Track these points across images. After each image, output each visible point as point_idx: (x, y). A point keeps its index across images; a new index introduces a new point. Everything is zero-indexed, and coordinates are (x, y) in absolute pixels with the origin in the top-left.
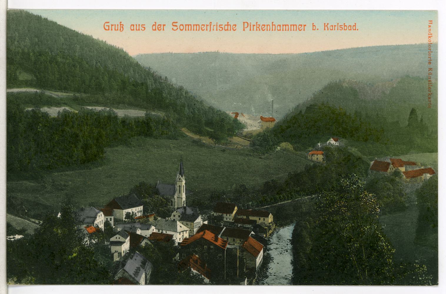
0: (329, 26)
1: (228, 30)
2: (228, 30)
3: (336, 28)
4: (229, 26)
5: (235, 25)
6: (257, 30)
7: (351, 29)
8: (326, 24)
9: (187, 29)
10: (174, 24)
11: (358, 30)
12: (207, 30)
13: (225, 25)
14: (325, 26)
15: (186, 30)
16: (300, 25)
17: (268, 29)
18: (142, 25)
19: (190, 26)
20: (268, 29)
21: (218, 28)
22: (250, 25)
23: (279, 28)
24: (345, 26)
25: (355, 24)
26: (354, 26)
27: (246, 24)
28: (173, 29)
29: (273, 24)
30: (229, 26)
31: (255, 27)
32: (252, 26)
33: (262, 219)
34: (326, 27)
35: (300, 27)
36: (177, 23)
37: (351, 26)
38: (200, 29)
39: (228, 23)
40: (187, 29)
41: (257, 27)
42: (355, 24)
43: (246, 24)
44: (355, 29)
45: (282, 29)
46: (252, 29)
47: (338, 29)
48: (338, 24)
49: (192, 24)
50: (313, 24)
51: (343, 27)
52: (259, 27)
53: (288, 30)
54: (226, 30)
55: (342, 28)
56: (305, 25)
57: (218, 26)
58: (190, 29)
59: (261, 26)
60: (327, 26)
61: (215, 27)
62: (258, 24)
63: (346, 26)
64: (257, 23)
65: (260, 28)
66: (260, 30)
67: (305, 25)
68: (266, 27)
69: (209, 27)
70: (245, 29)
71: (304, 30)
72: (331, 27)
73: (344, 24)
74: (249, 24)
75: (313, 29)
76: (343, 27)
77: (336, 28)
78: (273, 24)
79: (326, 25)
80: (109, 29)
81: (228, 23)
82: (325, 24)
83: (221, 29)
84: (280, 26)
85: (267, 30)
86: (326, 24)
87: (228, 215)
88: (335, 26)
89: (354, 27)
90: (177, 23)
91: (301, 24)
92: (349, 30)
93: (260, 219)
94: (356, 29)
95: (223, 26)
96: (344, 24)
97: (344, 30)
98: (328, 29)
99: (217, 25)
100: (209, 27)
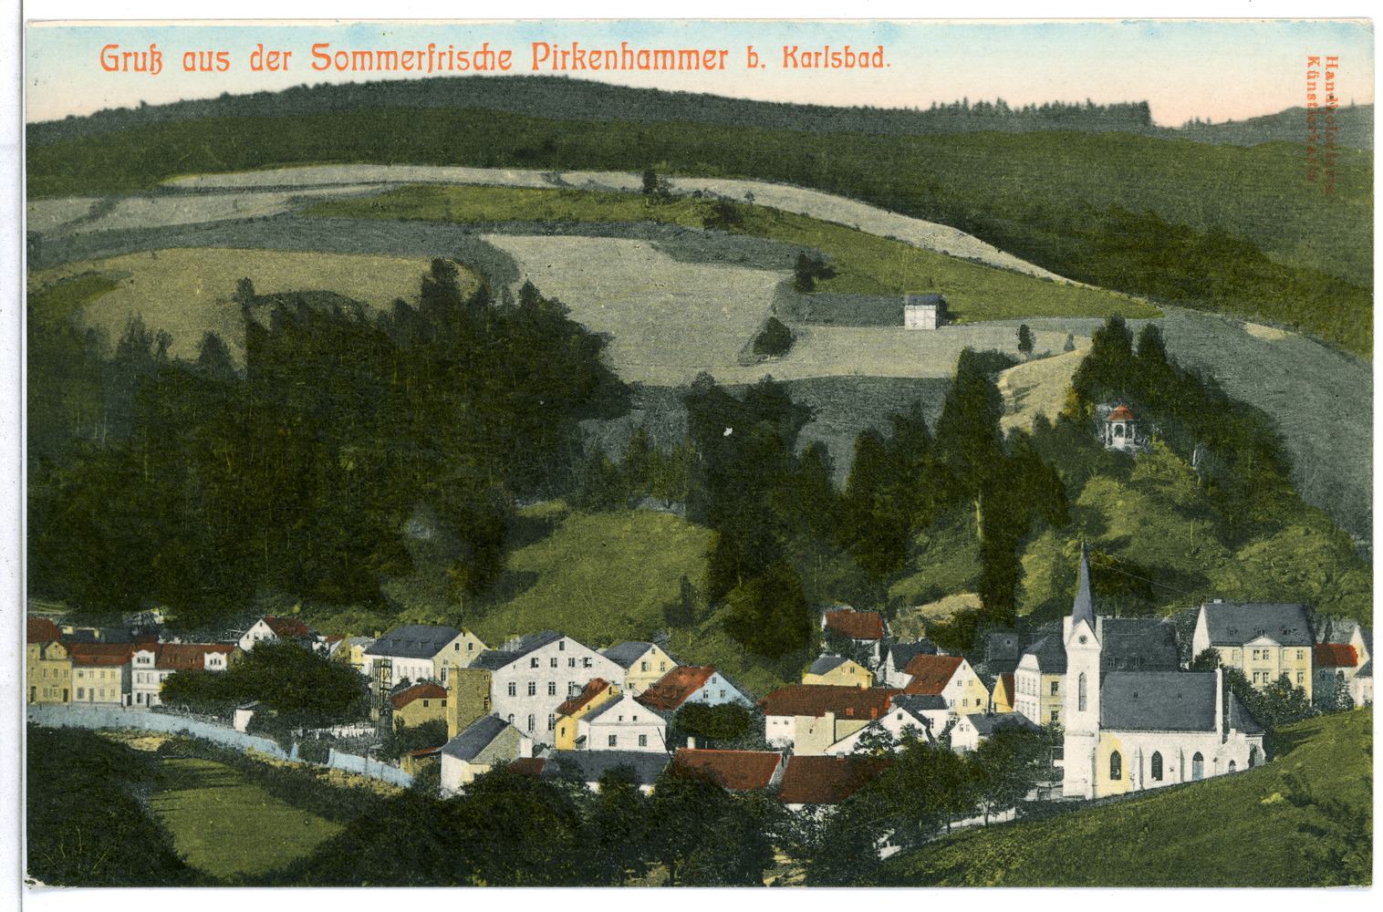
0: (798, 55)
2: (809, 65)
7: (867, 65)
10: (318, 50)
13: (477, 53)
14: (786, 55)
17: (611, 64)
18: (317, 45)
20: (611, 64)
22: (555, 52)
25: (881, 48)
26: (876, 54)
27: (541, 49)
29: (627, 48)
30: (489, 57)
32: (560, 56)
35: (709, 56)
36: (326, 45)
37: (867, 55)
38: (399, 63)
39: (486, 45)
40: (359, 65)
41: (575, 59)
42: (881, 48)
43: (541, 49)
45: (652, 65)
48: (827, 47)
50: (750, 48)
51: (842, 57)
52: (581, 59)
56: (723, 53)
58: (669, 63)
59: (588, 54)
60: (792, 54)
61: (446, 59)
63: (852, 54)
64: (575, 44)
66: (584, 67)
67: (723, 53)
68: (281, 60)
69: (425, 59)
71: (722, 67)
73: (847, 48)
74: (552, 49)
75: (750, 66)
76: (842, 57)
77: (821, 61)
78: (627, 48)
79: (789, 53)
80: (867, 65)
82: (786, 48)
85: (607, 67)
88: (817, 54)
90: (326, 45)
94: (885, 63)
95: (470, 58)
96: (847, 48)
97: (847, 65)
99: (451, 53)
100: (425, 59)
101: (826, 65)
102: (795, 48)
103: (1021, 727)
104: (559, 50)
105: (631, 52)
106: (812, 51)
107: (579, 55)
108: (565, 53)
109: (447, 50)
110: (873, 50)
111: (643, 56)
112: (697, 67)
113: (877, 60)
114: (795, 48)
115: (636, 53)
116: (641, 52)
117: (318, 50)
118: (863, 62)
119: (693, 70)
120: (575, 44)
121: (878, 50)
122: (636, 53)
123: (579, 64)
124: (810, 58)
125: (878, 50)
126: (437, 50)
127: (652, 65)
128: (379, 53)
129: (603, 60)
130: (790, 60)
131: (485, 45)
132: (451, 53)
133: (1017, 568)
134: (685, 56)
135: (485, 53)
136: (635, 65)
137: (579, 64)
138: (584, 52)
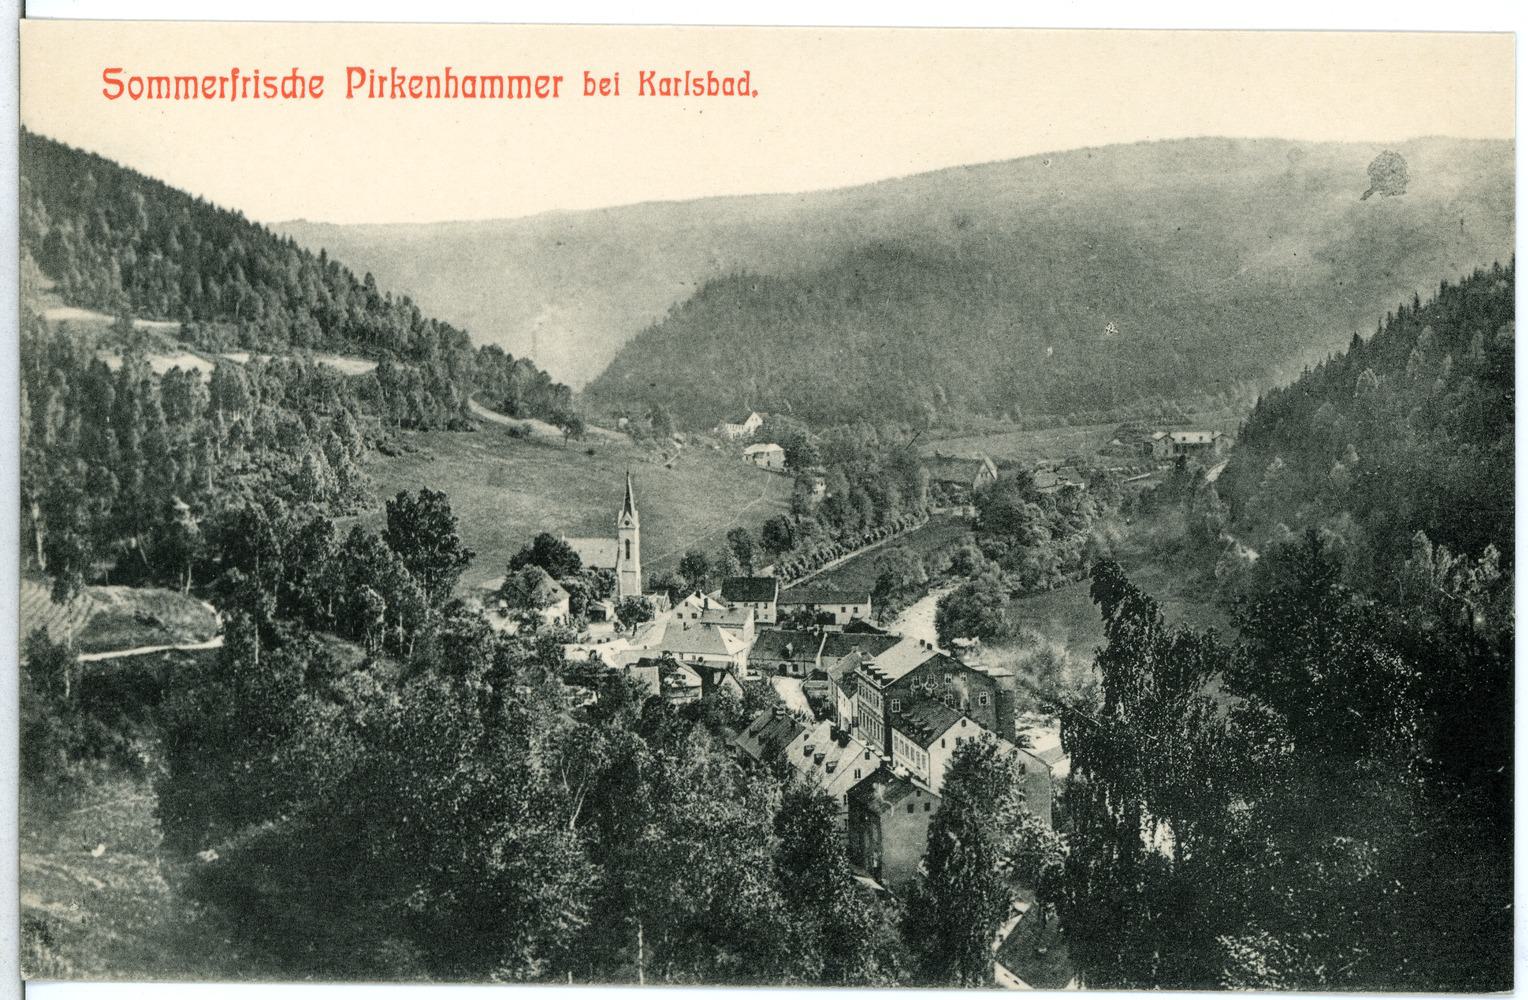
0: (656, 81)
1: (293, 94)
3: (682, 87)
4: (299, 82)
5: (321, 79)
6: (393, 95)
7: (732, 93)
8: (647, 75)
9: (155, 92)
10: (110, 76)
11: (755, 93)
12: (222, 95)
13: (285, 79)
14: (642, 82)
15: (150, 96)
16: (207, 78)
17: (434, 92)
18: (108, 71)
19: (164, 83)
20: (434, 92)
21: (262, 88)
23: (469, 89)
24: (711, 80)
25: (748, 73)
26: (742, 80)
28: (105, 92)
29: (452, 73)
31: (387, 85)
33: (850, 608)
34: (646, 85)
37: (732, 81)
39: (295, 70)
40: (155, 92)
41: (394, 86)
42: (748, 73)
43: (356, 78)
44: (747, 93)
45: (672, 91)
46: (377, 91)
47: (257, 95)
48: (688, 73)
49: (424, 75)
50: (586, 73)
51: (705, 83)
52: (400, 85)
53: (168, 96)
54: (286, 96)
55: (702, 87)
56: (557, 79)
57: (261, 82)
59: (407, 81)
60: (649, 80)
61: (251, 86)
62: (397, 73)
63: (715, 80)
64: (394, 70)
65: (405, 87)
66: (403, 95)
67: (557, 79)
69: (228, 86)
70: (354, 91)
72: (664, 85)
73: (710, 73)
75: (586, 93)
77: (682, 87)
79: (645, 79)
80: (732, 93)
81: (295, 70)
82: (642, 74)
83: (271, 92)
84: (473, 79)
85: (429, 95)
86: (647, 75)
87: (761, 605)
89: (743, 84)
91: (345, 74)
92: (726, 93)
93: (843, 610)
95: (277, 83)
96: (710, 73)
97: (710, 93)
98: (653, 93)
99: (257, 78)
100: (228, 86)
101: (687, 93)
102: (653, 74)
103: (455, 961)
104: (376, 75)
105: (456, 79)
106: (672, 76)
107: (397, 81)
108: (382, 79)
109: (251, 75)
110: (738, 75)
111: (469, 83)
112: (529, 95)
113: (743, 86)
114: (653, 74)
115: (307, 80)
116: (466, 78)
117: (110, 76)
118: (728, 89)
119: (524, 99)
120: (394, 70)
121: (744, 76)
122: (307, 80)
123: (398, 92)
124: (474, 84)
125: (744, 76)
126: (241, 75)
127: (672, 91)
128: (178, 79)
129: (424, 87)
130: (646, 86)
131: (295, 70)
132: (257, 78)
133: (25, 820)
134: (182, 83)
135: (294, 78)
136: (200, 94)
137: (398, 92)
138: (403, 78)
